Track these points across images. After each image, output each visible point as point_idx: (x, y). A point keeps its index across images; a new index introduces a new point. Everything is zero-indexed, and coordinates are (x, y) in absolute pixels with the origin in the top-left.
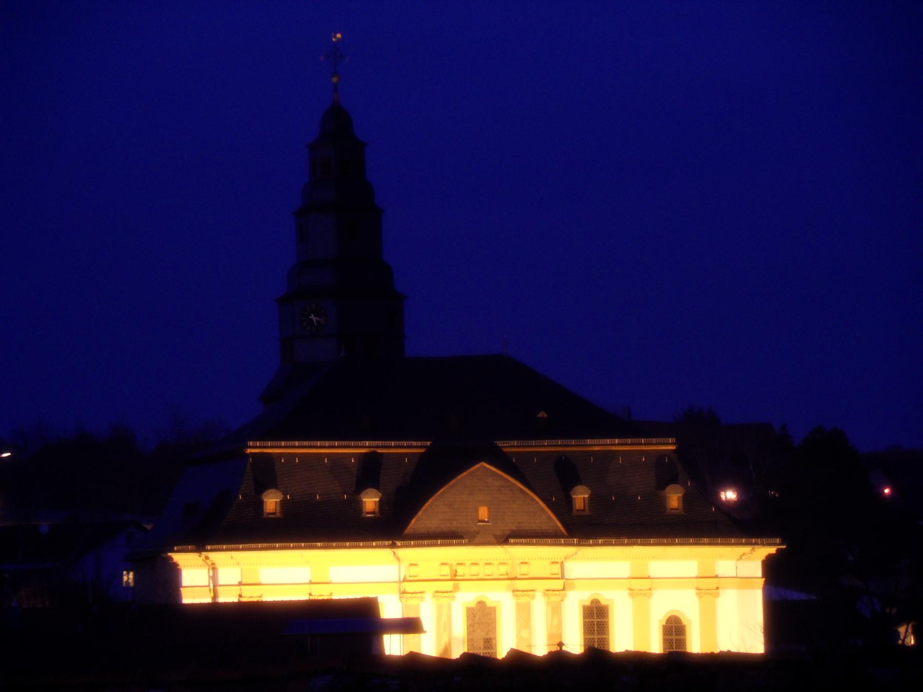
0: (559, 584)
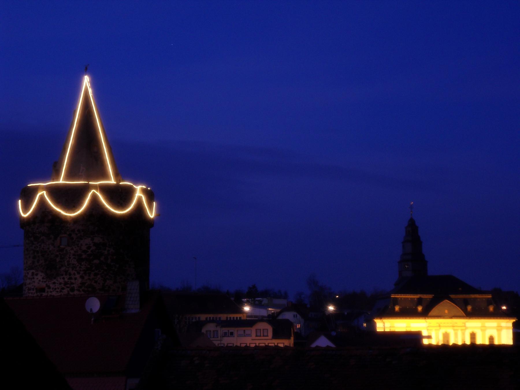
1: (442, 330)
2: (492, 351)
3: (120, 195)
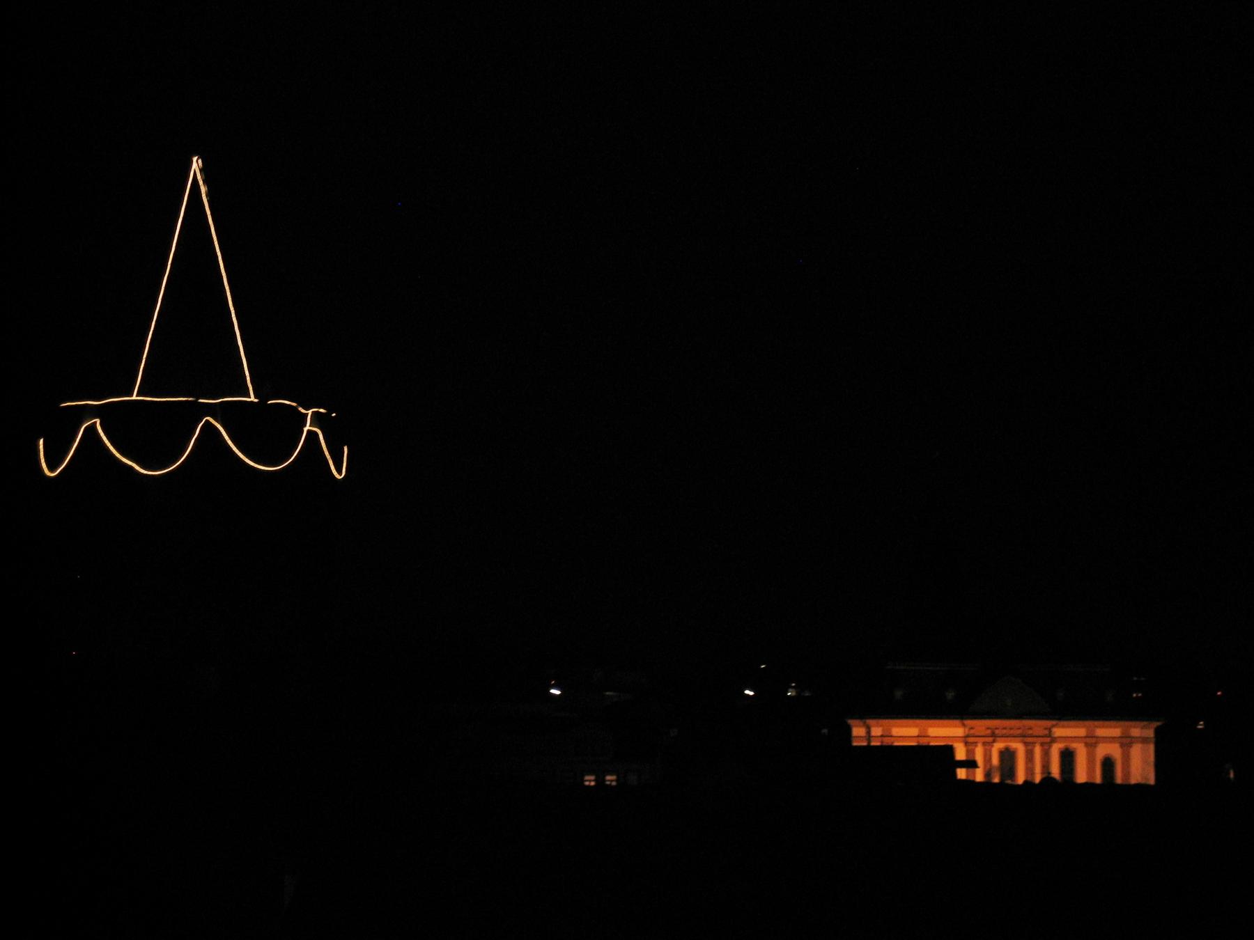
0: (1048, 740)
1: (978, 747)
2: (1109, 792)
3: (267, 430)
